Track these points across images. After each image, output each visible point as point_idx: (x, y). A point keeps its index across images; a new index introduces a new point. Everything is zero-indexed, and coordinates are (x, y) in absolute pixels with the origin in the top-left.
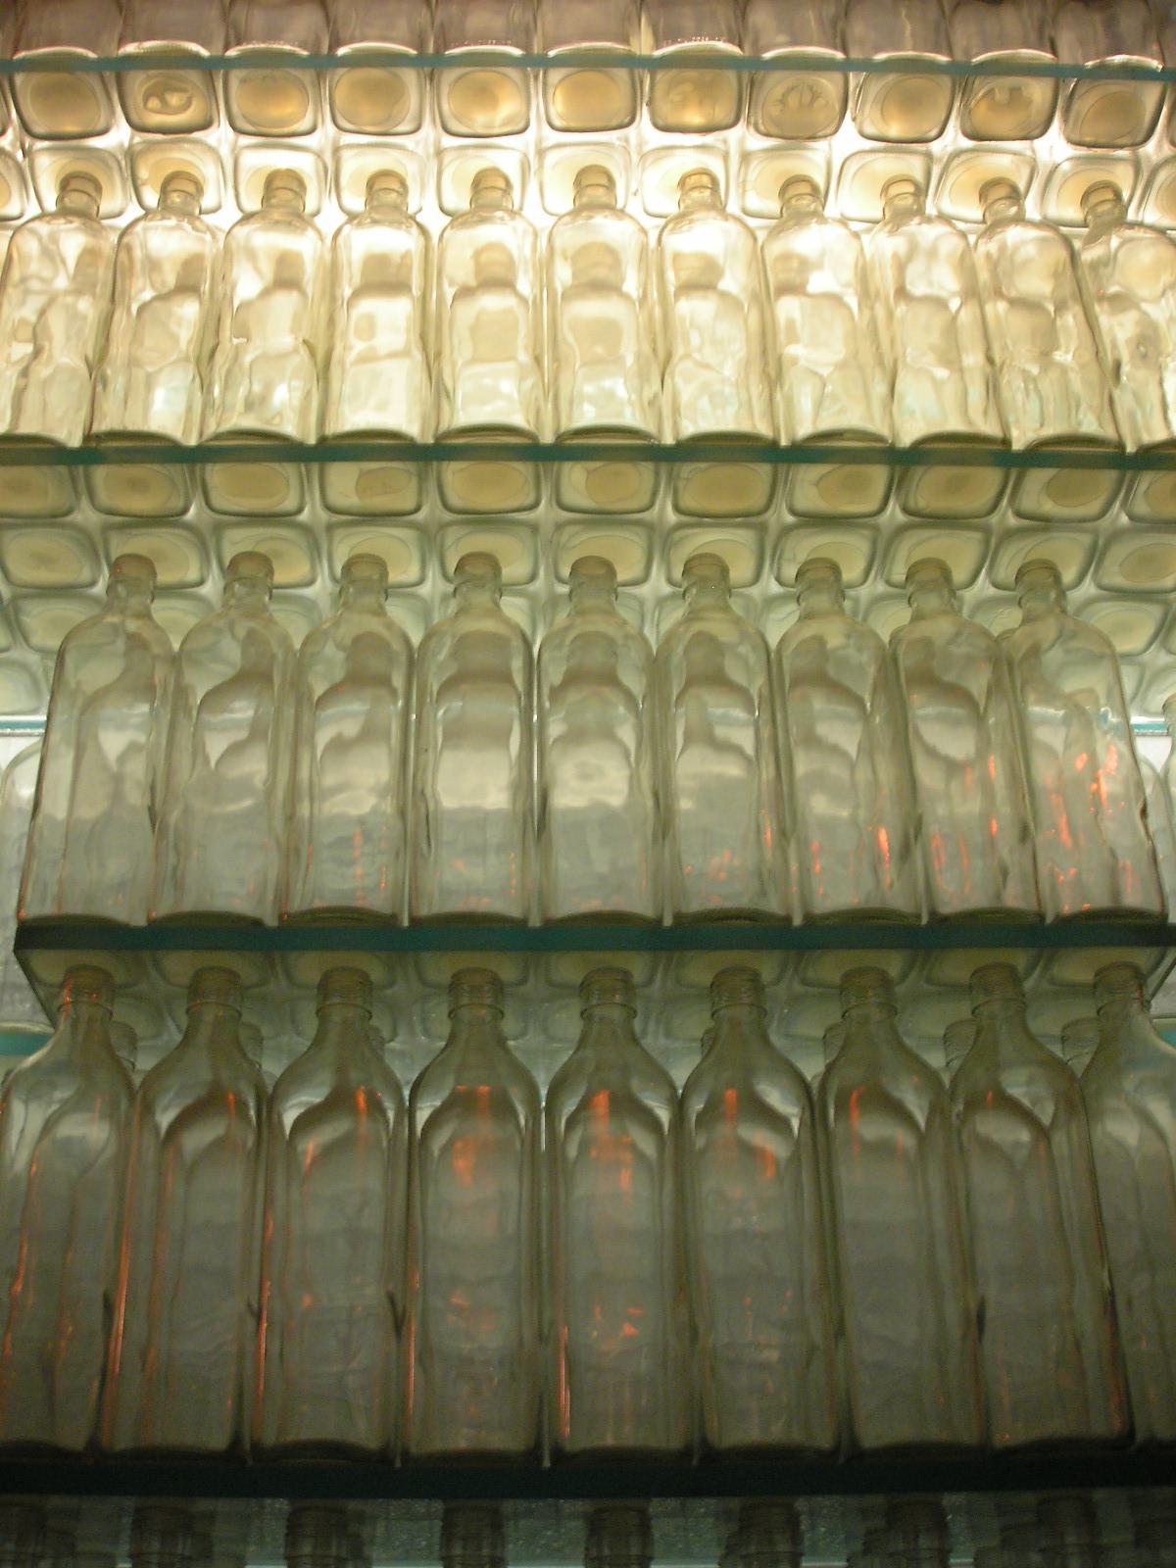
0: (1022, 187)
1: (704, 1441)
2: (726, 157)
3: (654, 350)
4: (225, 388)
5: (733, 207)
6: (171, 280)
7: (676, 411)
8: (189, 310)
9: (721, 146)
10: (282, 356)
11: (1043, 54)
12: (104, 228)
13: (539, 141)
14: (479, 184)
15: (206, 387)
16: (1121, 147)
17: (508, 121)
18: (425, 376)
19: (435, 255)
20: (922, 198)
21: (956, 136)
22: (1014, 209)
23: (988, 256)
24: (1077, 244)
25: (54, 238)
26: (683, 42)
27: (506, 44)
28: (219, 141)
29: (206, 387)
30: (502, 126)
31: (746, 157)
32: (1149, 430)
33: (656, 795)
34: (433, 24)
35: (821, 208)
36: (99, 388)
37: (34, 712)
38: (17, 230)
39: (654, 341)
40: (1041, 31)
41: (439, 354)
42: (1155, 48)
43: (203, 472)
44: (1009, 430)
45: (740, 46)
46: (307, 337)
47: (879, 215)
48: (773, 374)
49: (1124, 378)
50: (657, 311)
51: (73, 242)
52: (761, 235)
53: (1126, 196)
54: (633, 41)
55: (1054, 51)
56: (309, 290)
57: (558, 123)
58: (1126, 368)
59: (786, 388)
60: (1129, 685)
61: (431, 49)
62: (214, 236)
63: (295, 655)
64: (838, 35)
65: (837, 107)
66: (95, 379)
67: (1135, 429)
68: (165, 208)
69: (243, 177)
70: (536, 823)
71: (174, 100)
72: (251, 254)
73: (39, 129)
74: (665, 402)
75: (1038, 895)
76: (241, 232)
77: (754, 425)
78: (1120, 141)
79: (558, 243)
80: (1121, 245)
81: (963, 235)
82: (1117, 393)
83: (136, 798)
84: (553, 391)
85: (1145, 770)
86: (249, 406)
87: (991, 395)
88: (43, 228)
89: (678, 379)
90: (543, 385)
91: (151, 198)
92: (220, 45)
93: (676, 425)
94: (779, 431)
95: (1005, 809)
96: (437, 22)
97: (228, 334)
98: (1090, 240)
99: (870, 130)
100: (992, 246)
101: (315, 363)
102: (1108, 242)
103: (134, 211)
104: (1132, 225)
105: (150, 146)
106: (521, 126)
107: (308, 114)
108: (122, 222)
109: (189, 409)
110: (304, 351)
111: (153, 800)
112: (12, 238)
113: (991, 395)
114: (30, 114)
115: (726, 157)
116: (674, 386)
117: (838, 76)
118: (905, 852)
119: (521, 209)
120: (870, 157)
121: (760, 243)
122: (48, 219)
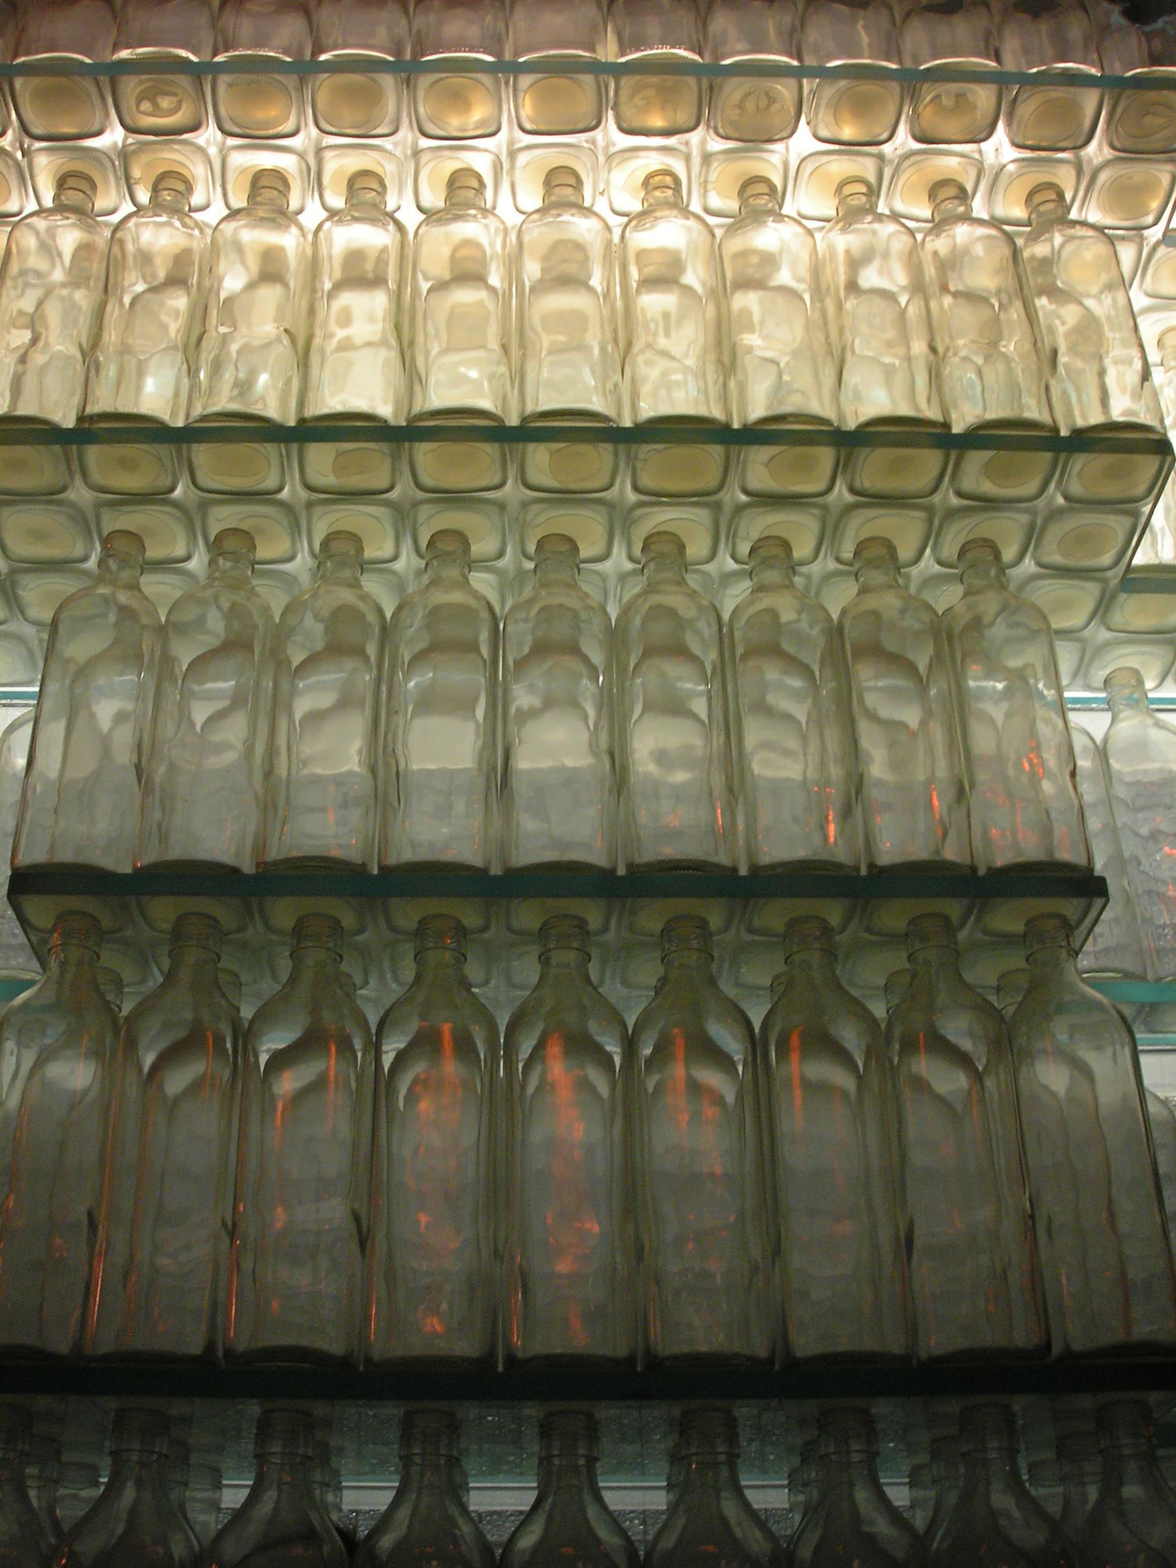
0: (969, 188)
2: (688, 159)
7: (635, 396)
8: (180, 302)
13: (511, 143)
16: (1063, 150)
17: (481, 123)
19: (410, 252)
20: (874, 199)
24: (1020, 242)
25: (51, 232)
28: (208, 141)
30: (474, 129)
31: (707, 158)
39: (615, 331)
46: (288, 327)
50: (619, 303)
51: (69, 238)
52: (719, 233)
53: (1068, 197)
55: (998, 59)
58: (1063, 359)
67: (1069, 412)
68: (157, 205)
71: (165, 103)
72: (239, 248)
73: (38, 131)
74: (625, 387)
76: (229, 228)
77: (711, 412)
79: (526, 239)
81: (911, 232)
88: (41, 223)
92: (209, 52)
97: (214, 322)
98: (1033, 238)
99: (824, 133)
101: (297, 353)
102: (1051, 240)
104: (1075, 223)
108: (115, 219)
109: (177, 394)
110: (286, 340)
115: (688, 159)
117: (792, 82)
120: (825, 159)
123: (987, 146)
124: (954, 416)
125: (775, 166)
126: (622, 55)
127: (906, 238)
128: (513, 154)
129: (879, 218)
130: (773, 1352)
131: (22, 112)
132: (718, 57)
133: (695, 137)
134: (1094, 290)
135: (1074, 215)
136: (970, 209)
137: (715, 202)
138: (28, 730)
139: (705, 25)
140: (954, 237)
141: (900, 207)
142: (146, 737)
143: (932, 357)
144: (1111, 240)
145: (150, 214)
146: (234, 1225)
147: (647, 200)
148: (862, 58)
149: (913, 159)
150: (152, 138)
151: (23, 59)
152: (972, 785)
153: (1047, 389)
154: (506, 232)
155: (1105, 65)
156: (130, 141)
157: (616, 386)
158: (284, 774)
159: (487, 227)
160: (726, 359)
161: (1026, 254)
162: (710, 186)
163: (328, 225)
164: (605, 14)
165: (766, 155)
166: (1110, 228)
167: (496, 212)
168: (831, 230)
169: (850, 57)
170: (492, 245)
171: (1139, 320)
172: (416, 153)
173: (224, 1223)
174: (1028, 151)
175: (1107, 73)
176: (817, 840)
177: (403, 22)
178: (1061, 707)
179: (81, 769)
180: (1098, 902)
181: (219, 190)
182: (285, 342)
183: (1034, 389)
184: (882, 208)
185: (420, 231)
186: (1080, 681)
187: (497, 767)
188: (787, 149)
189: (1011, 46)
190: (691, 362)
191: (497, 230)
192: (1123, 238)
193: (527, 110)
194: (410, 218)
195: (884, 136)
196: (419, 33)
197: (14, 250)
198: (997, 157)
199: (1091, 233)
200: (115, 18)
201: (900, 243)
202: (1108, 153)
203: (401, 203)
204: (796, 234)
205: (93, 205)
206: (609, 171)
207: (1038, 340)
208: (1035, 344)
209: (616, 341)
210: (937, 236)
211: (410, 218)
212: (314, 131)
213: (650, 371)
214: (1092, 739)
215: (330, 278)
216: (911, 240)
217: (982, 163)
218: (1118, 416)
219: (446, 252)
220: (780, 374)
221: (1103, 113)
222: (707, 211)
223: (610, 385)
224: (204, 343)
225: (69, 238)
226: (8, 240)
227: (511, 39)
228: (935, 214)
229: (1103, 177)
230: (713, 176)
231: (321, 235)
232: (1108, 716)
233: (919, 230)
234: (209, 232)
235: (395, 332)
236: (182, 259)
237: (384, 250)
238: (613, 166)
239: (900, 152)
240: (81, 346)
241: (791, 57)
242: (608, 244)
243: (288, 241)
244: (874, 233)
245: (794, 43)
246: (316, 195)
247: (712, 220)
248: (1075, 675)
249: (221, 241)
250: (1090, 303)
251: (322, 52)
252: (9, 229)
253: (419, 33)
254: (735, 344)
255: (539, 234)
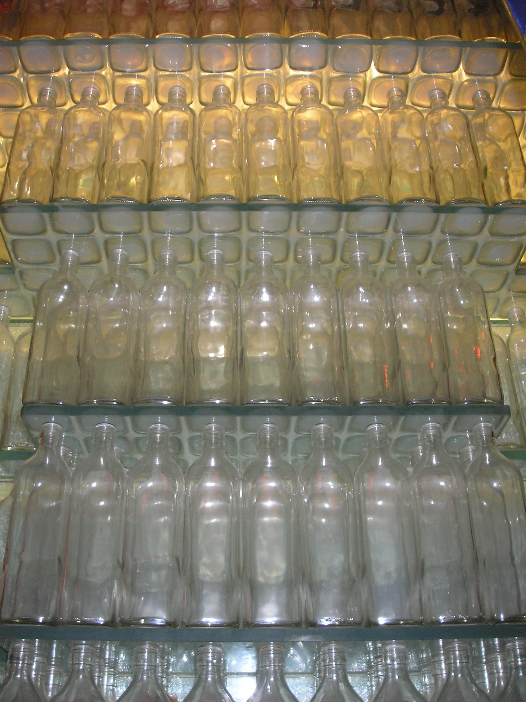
0: (447, 93)
1: (307, 618)
2: (321, 81)
3: (290, 164)
4: (109, 180)
5: (324, 102)
6: (86, 132)
7: (299, 189)
8: (94, 145)
9: (318, 75)
10: (132, 165)
11: (456, 37)
12: (57, 110)
13: (242, 73)
14: (216, 93)
15: (101, 180)
16: (489, 76)
17: (228, 65)
18: (193, 174)
19: (197, 122)
20: (404, 98)
21: (419, 71)
22: (444, 102)
23: (432, 121)
24: (470, 117)
25: (37, 116)
26: (302, 32)
27: (228, 34)
28: (106, 73)
29: (101, 180)
30: (226, 67)
31: (330, 80)
32: (499, 196)
33: (289, 352)
34: (197, 22)
35: (361, 102)
36: (56, 180)
37: (28, 315)
38: (22, 111)
39: (289, 160)
40: (455, 27)
41: (198, 165)
42: (503, 34)
43: (219, 656)
44: (438, 196)
45: (327, 34)
46: (143, 158)
47: (386, 104)
48: (339, 173)
49: (489, 175)
50: (291, 145)
51: (44, 118)
52: (335, 114)
53: (491, 96)
54: (282, 32)
55: (460, 36)
56: (145, 136)
57: (250, 66)
58: (490, 170)
59: (345, 178)
60: (490, 306)
61: (196, 35)
62: (103, 114)
63: (305, 504)
64: (369, 29)
65: (368, 60)
66: (54, 176)
67: (493, 195)
68: (84, 101)
69: (117, 90)
70: (239, 364)
71: (87, 57)
72: (120, 121)
73: (31, 69)
74: (294, 184)
75: (449, 393)
76: (116, 113)
77: (332, 196)
78: (489, 73)
79: (250, 117)
80: (489, 118)
81: (420, 112)
82: (485, 181)
83: (72, 352)
84: (247, 181)
85: (496, 341)
86: (119, 186)
87: (432, 183)
88: (32, 111)
89: (300, 176)
90: (243, 177)
91: (78, 98)
92: (106, 34)
93: (298, 194)
94: (342, 198)
95: (436, 356)
96: (199, 23)
97: (110, 157)
98: (476, 115)
99: (382, 69)
100: (434, 118)
101: (147, 169)
102: (484, 116)
103: (70, 104)
104: (494, 109)
105: (77, 77)
106: (234, 67)
107: (144, 63)
108: (67, 107)
109: (94, 188)
110: (142, 164)
111: (79, 353)
112: (19, 115)
113: (432, 183)
114: (27, 63)
115: (321, 81)
116: (298, 178)
117: (368, 47)
118: (394, 376)
119: (234, 102)
120: (382, 80)
121: (335, 117)
122: (34, 107)
123: (455, 74)
124: (441, 197)
125: (360, 83)
126: (292, 35)
127: (418, 115)
128: (243, 79)
129: (407, 107)
130: (362, 618)
131: (23, 59)
132: (334, 36)
133: (324, 71)
134: (503, 137)
135: (494, 105)
136: (447, 102)
137: (333, 99)
138: (29, 336)
139: (329, 21)
140: (440, 115)
141: (416, 101)
142: (81, 345)
143: (431, 171)
144: (510, 116)
145: (81, 106)
146: (123, 564)
147: (303, 99)
148: (400, 35)
149: (422, 80)
150: (81, 72)
151: (24, 38)
152: (449, 364)
153: (483, 185)
154: (240, 114)
155: (508, 38)
156: (72, 73)
157: (290, 184)
158: (143, 359)
159: (231, 111)
160: (339, 171)
161: (473, 122)
162: (331, 92)
163: (160, 111)
164: (284, 16)
165: (356, 79)
166: (510, 110)
167: (236, 105)
168: (385, 112)
169: (393, 35)
170: (234, 119)
171: (523, 150)
172: (200, 79)
173: (119, 563)
174: (474, 76)
175: (510, 41)
176: (380, 389)
177: (193, 19)
178: (489, 323)
179: (53, 355)
180: (506, 417)
181: (111, 95)
182: (141, 164)
183: (477, 184)
184: (408, 103)
185: (202, 114)
186: (496, 313)
187: (238, 357)
188: (365, 75)
189: (466, 28)
190: (322, 172)
191: (236, 112)
192: (516, 115)
193: (249, 60)
194: (196, 106)
195: (409, 70)
196: (200, 25)
197: (20, 123)
198: (459, 79)
199: (501, 113)
200: (65, 18)
201: (416, 118)
202: (509, 77)
203: (192, 100)
204: (369, 114)
205: (55, 102)
206: (286, 86)
207: (479, 163)
208: (477, 164)
209: (290, 164)
210: (433, 115)
211: (196, 106)
212: (153, 68)
213: (304, 179)
214: (502, 340)
215: (162, 135)
216: (421, 117)
217: (452, 81)
218: (514, 197)
219: (212, 121)
220: (363, 177)
221: (508, 59)
222: (330, 104)
223: (287, 183)
224: (106, 165)
225: (44, 118)
226: (18, 119)
227: (242, 28)
228: (432, 105)
229: (507, 88)
230: (332, 88)
231: (158, 116)
232: (509, 329)
233: (425, 111)
234: (108, 114)
235: (191, 161)
236: (94, 126)
237: (186, 121)
238: (288, 83)
239: (416, 77)
240: (51, 167)
241: (367, 34)
242: (286, 119)
243: (142, 118)
244: (404, 113)
245: (369, 29)
246: (155, 98)
247: (331, 107)
248: (495, 309)
249: (113, 118)
250: (500, 144)
251: (157, 34)
252: (19, 113)
253: (200, 25)
254: (343, 166)
255: (254, 115)
